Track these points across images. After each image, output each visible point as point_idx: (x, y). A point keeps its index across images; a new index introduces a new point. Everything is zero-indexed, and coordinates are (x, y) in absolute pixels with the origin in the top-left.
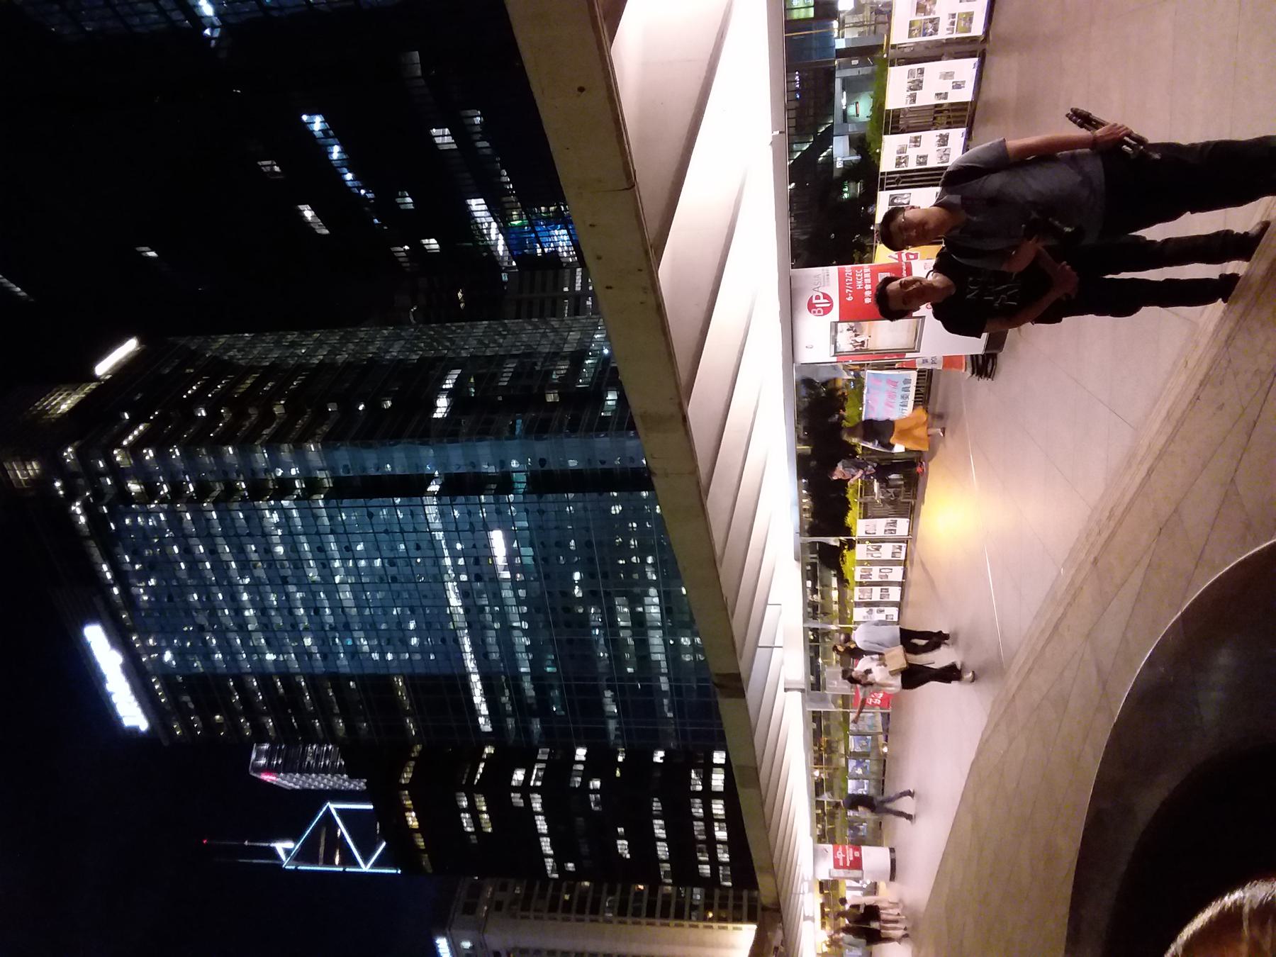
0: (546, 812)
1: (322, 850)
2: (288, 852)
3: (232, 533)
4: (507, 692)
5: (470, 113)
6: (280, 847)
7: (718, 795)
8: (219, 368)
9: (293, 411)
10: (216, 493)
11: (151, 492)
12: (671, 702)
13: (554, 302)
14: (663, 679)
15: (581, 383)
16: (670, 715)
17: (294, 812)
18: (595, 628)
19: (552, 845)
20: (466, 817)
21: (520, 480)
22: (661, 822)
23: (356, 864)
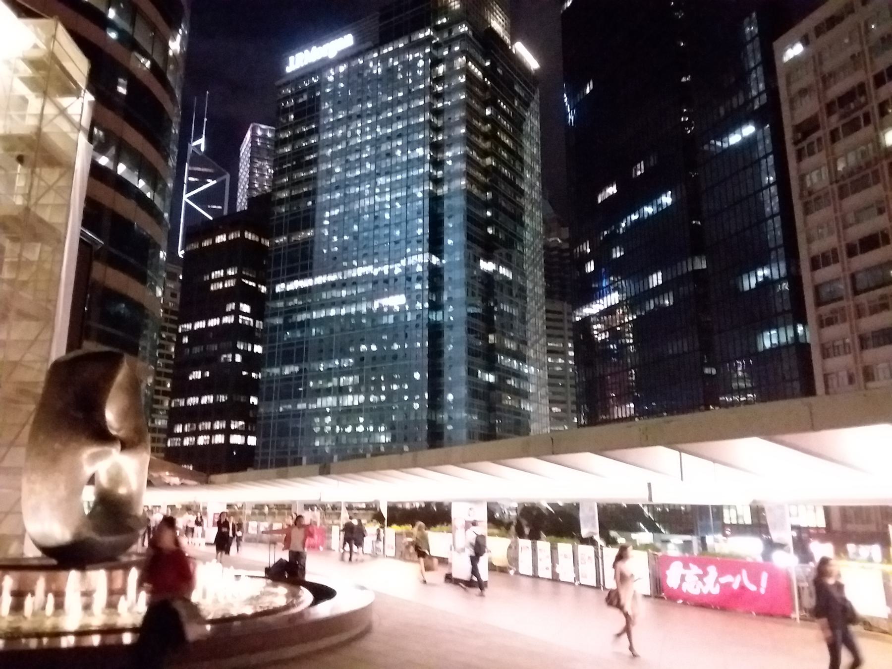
1: (199, 169)
2: (198, 147)
3: (410, 113)
4: (301, 303)
6: (201, 142)
7: (227, 439)
8: (518, 122)
9: (486, 171)
11: (438, 80)
12: (289, 411)
13: (561, 336)
15: (501, 358)
16: (281, 409)
18: (340, 362)
19: (200, 329)
20: (221, 273)
21: (438, 316)
23: (188, 191)
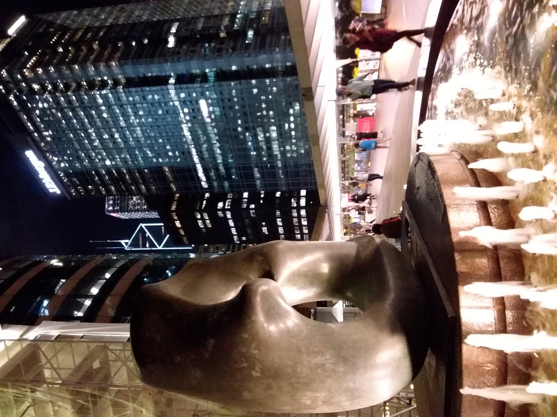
0: (233, 218)
1: (141, 242)
2: (126, 243)
4: (213, 171)
6: (123, 242)
7: (303, 208)
9: (103, 47)
10: (73, 88)
11: (44, 89)
12: (283, 171)
16: (282, 177)
17: (127, 228)
19: (236, 231)
22: (280, 219)
23: (156, 247)
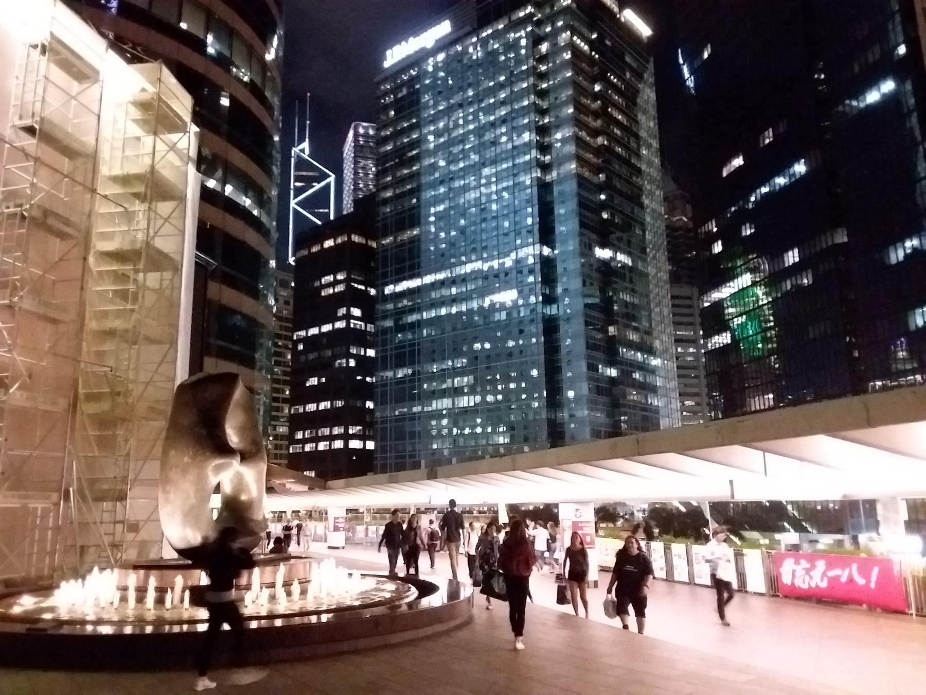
1: (304, 173)
2: (303, 151)
4: (410, 304)
5: (810, 276)
6: (306, 145)
8: (631, 96)
9: (598, 151)
11: (542, 59)
14: (420, 408)
15: (623, 350)
18: (453, 362)
19: (314, 336)
20: (330, 278)
21: (552, 310)
22: (329, 406)
23: (296, 197)
